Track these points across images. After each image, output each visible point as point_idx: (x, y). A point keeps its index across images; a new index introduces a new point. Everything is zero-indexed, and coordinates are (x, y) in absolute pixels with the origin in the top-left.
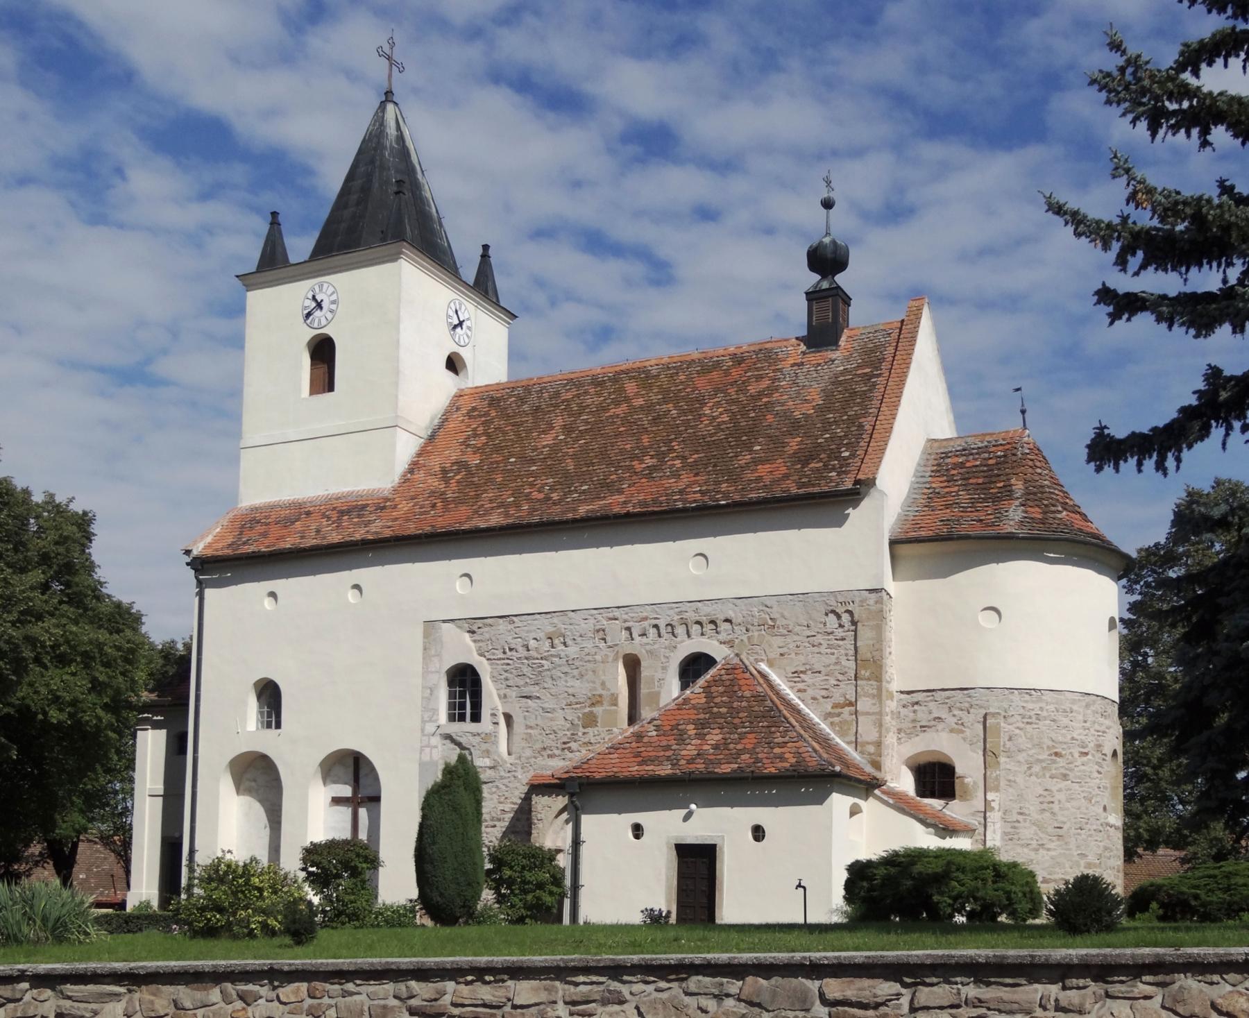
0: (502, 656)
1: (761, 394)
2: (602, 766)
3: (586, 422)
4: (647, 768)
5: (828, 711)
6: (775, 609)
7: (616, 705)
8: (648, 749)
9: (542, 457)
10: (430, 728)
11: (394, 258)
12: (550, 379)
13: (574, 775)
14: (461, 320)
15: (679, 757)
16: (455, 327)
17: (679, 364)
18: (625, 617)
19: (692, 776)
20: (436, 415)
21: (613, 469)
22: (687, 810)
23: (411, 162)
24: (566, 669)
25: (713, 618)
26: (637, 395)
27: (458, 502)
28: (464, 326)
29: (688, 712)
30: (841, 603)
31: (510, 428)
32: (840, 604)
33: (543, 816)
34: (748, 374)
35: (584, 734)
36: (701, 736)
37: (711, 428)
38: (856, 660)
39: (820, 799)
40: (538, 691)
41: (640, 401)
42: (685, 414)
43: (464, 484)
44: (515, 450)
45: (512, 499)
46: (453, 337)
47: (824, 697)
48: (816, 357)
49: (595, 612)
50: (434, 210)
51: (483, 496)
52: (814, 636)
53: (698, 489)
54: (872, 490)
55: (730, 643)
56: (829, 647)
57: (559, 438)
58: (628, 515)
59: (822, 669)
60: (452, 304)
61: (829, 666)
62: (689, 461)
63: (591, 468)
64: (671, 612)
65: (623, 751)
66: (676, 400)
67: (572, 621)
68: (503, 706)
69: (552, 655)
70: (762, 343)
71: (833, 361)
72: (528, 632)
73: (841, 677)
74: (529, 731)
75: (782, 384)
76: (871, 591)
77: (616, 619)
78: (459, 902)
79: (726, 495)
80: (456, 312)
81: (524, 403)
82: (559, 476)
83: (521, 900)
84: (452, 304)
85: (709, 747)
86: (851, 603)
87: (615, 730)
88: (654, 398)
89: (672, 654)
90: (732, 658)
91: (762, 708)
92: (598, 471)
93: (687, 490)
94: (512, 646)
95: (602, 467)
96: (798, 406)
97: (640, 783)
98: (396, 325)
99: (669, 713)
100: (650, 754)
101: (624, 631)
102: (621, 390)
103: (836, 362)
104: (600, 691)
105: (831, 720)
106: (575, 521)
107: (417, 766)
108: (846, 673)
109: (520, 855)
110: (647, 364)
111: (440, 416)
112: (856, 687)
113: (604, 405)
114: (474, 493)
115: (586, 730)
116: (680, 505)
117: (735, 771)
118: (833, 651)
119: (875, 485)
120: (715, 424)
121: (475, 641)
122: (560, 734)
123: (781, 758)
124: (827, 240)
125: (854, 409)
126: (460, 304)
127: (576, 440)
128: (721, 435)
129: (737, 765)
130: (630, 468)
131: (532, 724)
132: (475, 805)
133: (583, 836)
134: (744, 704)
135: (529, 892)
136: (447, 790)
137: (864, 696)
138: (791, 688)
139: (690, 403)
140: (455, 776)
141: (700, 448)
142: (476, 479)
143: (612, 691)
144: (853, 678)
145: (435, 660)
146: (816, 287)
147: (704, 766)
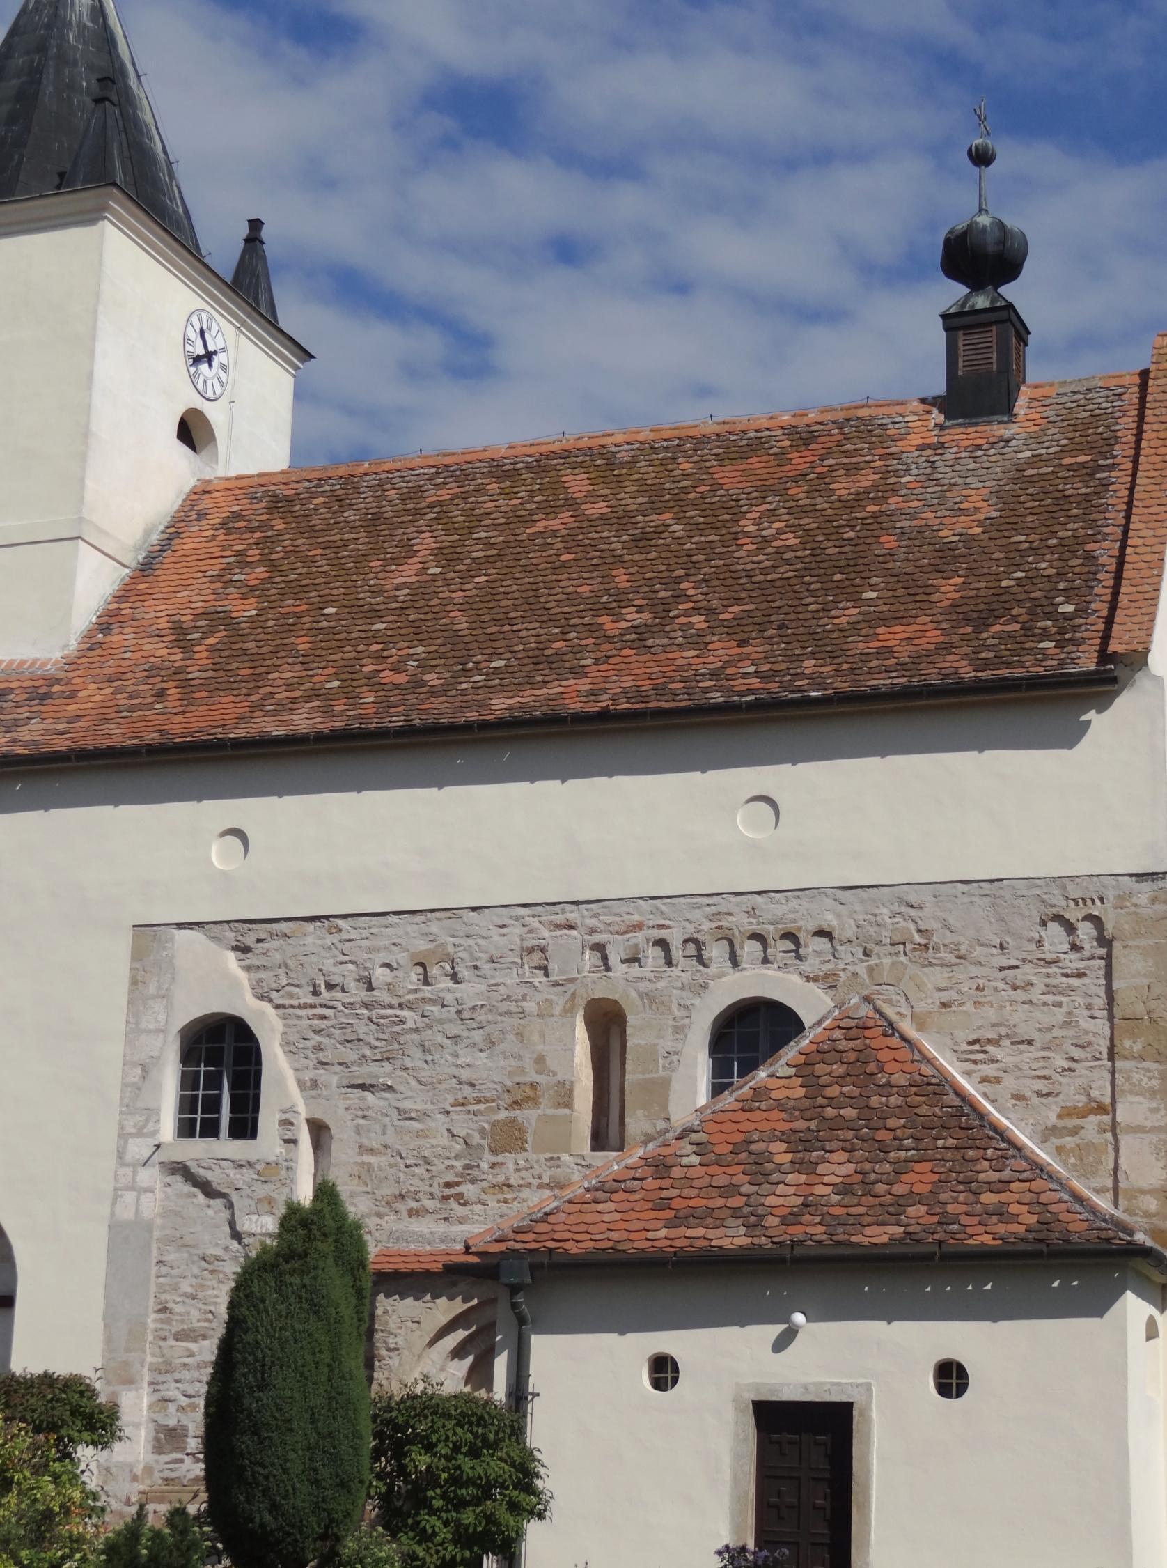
0: (310, 1000)
1: (860, 499)
2: (583, 1228)
3: (487, 544)
4: (690, 1233)
5: (1050, 1125)
6: (929, 910)
7: (569, 1105)
8: (685, 1193)
9: (395, 605)
10: (139, 1149)
11: (90, 217)
12: (398, 465)
13: (518, 1246)
14: (211, 349)
15: (760, 1211)
16: (197, 360)
17: (676, 442)
18: (592, 922)
19: (798, 1251)
20: (155, 526)
21: (556, 630)
22: (782, 1327)
23: (119, 57)
24: (455, 1029)
25: (790, 927)
26: (591, 496)
27: (216, 686)
28: (215, 364)
29: (765, 1115)
30: (1075, 901)
31: (320, 551)
32: (1071, 903)
33: (400, 1341)
34: (826, 463)
35: (493, 1165)
36: (808, 1168)
37: (761, 558)
38: (1111, 1018)
39: (1098, 1306)
40: (389, 1075)
41: (600, 508)
42: (701, 530)
43: (227, 653)
44: (335, 592)
45: (337, 683)
46: (193, 378)
47: (1039, 1094)
48: (965, 435)
49: (523, 911)
50: (159, 148)
51: (270, 677)
52: (1017, 967)
53: (753, 669)
54: (1138, 675)
55: (828, 981)
56: (1050, 989)
57: (430, 571)
58: (604, 716)
59: (1036, 1036)
60: (194, 319)
61: (1050, 1029)
62: (722, 617)
63: (507, 628)
64: (696, 915)
65: (625, 1196)
66: (680, 506)
67: (470, 930)
68: (306, 1105)
69: (423, 1000)
70: (848, 409)
71: (1007, 441)
72: (370, 950)
73: (1077, 1053)
74: (367, 1158)
75: (903, 480)
76: (1140, 877)
77: (572, 927)
78: (314, 1525)
79: (817, 680)
80: (202, 333)
81: (343, 508)
82: (439, 641)
83: (446, 1523)
84: (194, 319)
85: (828, 1190)
86: (1098, 902)
87: (565, 1157)
88: (631, 504)
89: (697, 1001)
90: (857, 1007)
91: (937, 1109)
92: (524, 633)
93: (729, 671)
94: (336, 979)
95: (530, 626)
96: (945, 521)
97: (675, 1264)
98: (86, 344)
99: (721, 1117)
100: (692, 1203)
101: (588, 952)
102: (557, 486)
103: (1013, 443)
104: (533, 1077)
105: (1058, 1142)
106: (484, 725)
107: (103, 1231)
108: (1089, 1044)
109: (449, 1417)
110: (608, 441)
111: (162, 528)
112: (1113, 1073)
113: (522, 513)
114: (250, 671)
115: (499, 1159)
116: (717, 698)
117: (900, 1240)
118: (1059, 998)
119: (1146, 664)
120: (770, 550)
121: (248, 969)
122: (439, 1165)
123: (1001, 1213)
124: (984, 220)
125: (1070, 526)
126: (210, 320)
127: (469, 575)
128: (786, 571)
129: (902, 1229)
130: (593, 629)
131: (374, 1145)
132: (354, 1301)
133: (535, 1382)
134: (895, 1100)
135: (468, 1504)
136: (296, 1264)
137: (1131, 1092)
138: (967, 1074)
139: (708, 512)
140: (318, 1233)
141: (743, 594)
142: (252, 645)
143: (560, 1077)
144: (1105, 1056)
145: (158, 1006)
146: (964, 305)
147: (822, 1229)
